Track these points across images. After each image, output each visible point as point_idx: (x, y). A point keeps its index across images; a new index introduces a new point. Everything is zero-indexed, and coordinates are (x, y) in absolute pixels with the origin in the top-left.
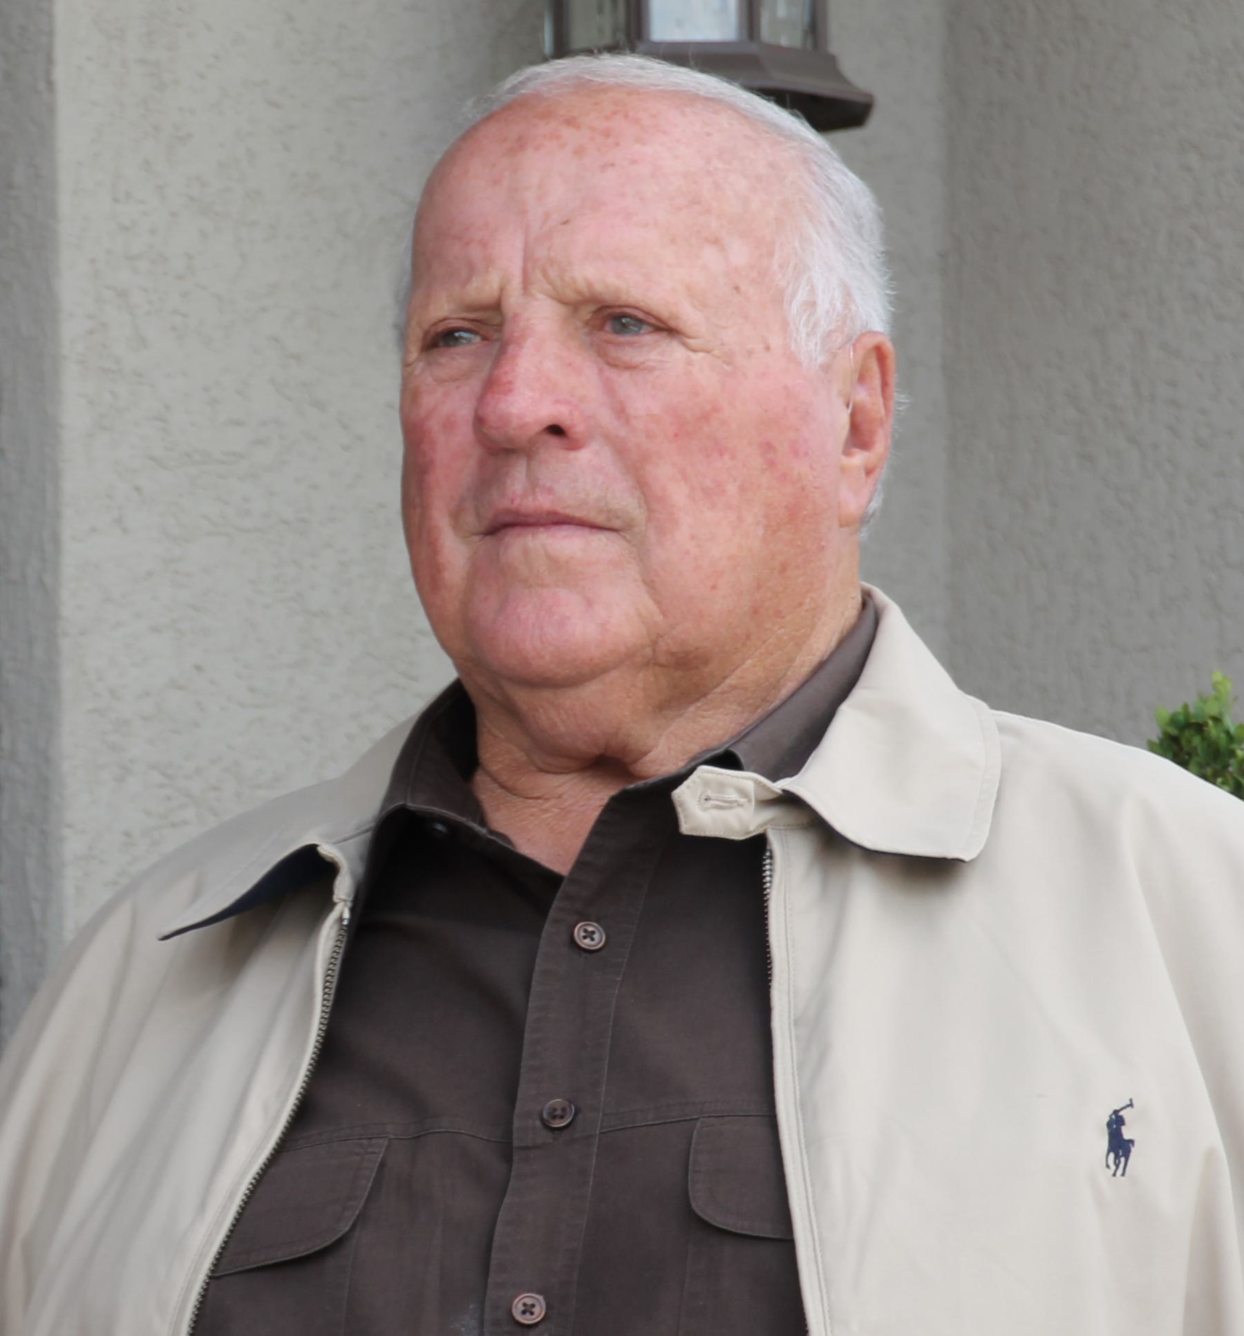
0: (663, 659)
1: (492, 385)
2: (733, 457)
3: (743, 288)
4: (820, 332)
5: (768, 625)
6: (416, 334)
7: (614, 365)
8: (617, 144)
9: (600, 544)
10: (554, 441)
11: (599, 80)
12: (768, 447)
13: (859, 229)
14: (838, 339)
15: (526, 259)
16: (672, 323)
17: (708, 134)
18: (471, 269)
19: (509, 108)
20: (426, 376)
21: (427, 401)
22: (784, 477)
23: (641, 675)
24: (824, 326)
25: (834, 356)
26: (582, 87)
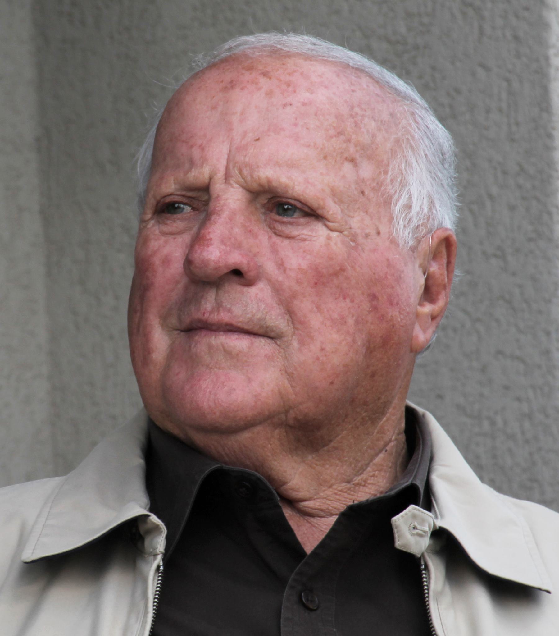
0: (291, 422)
1: (198, 239)
2: (352, 301)
3: (366, 193)
4: (412, 225)
5: (358, 410)
6: (151, 202)
7: (279, 235)
8: (295, 92)
9: (263, 346)
10: (235, 278)
11: (287, 49)
12: (373, 297)
13: (443, 162)
14: (424, 231)
15: (228, 160)
16: (320, 212)
17: (353, 91)
18: (192, 163)
19: (225, 61)
20: (154, 228)
21: (154, 244)
22: (382, 318)
23: (277, 431)
24: (415, 222)
25: (419, 241)
26: (276, 53)
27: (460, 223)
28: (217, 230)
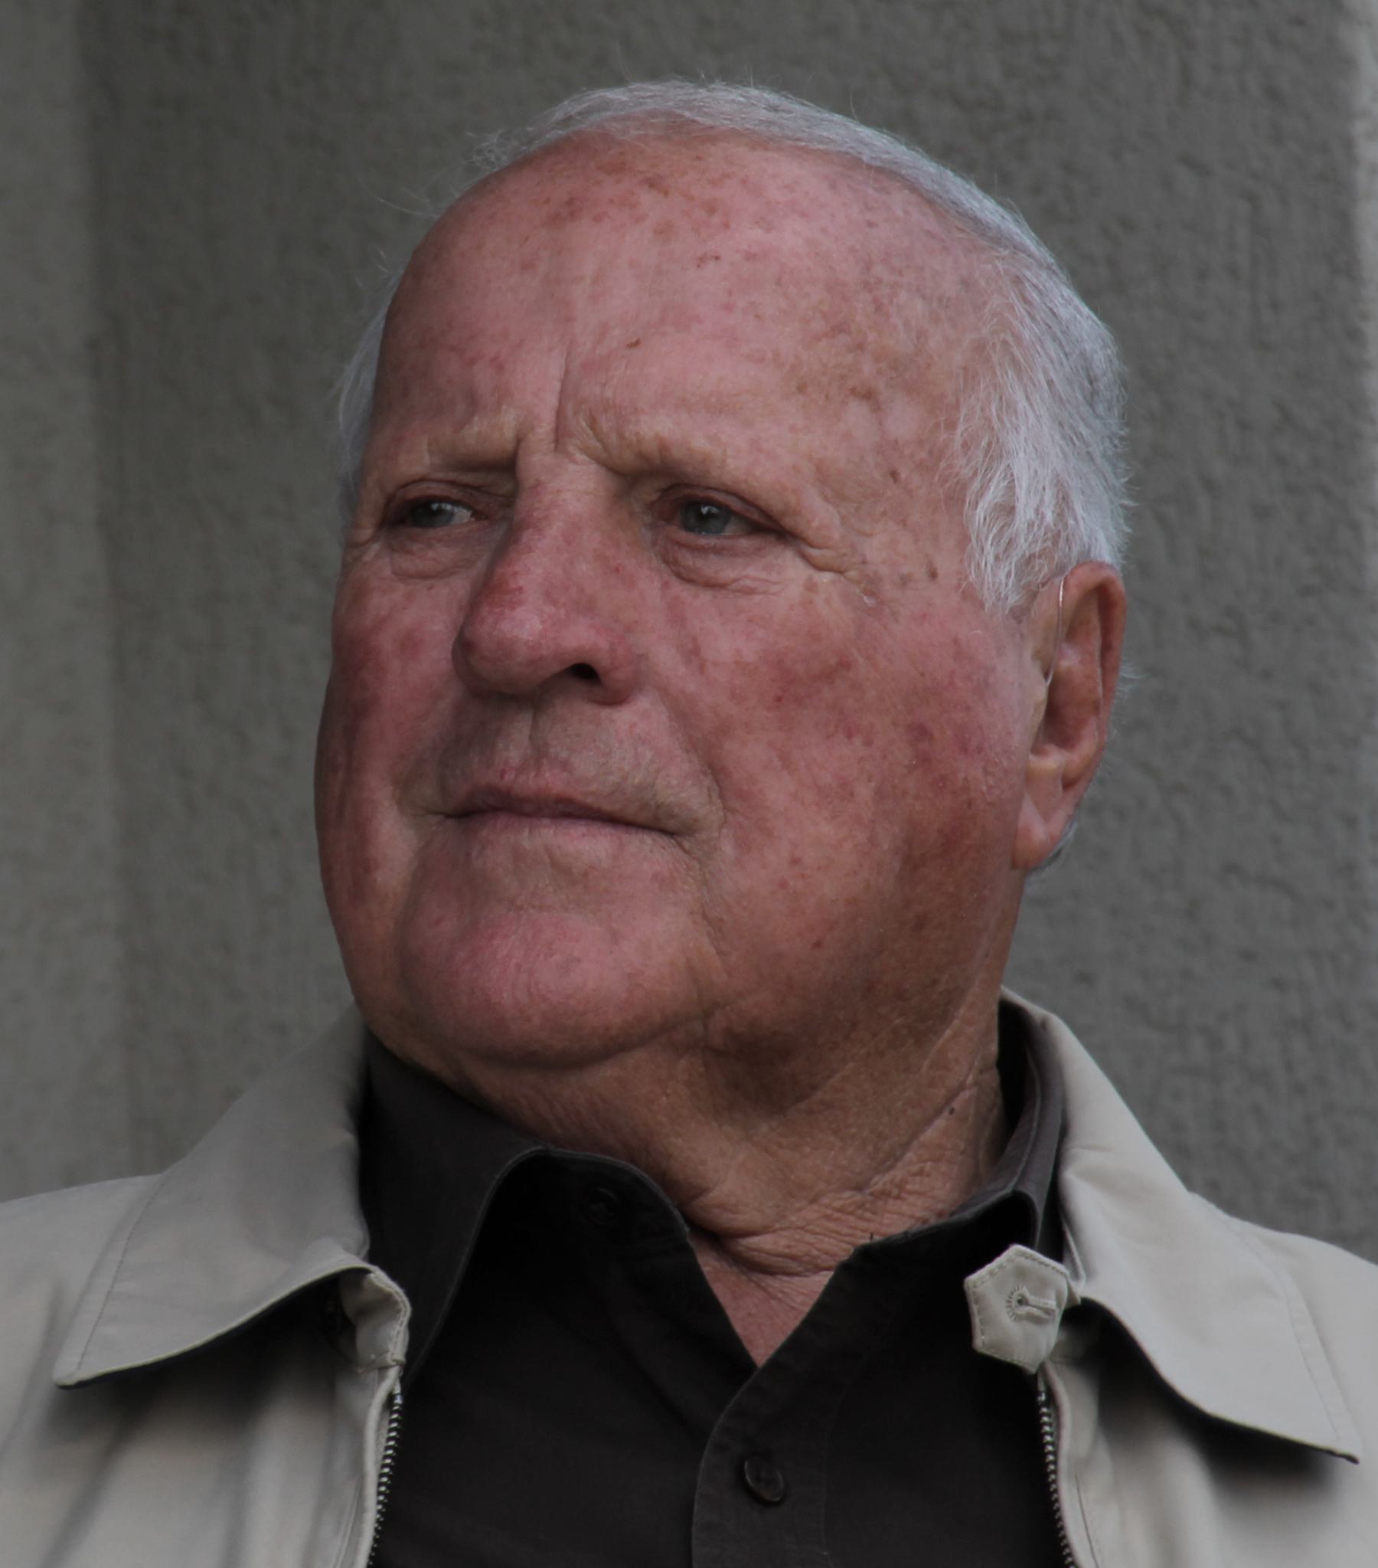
1: (489, 590)
2: (868, 743)
4: (1016, 556)
6: (373, 499)
7: (687, 578)
8: (727, 226)
9: (648, 854)
11: (708, 122)
12: (920, 732)
15: (563, 395)
16: (788, 522)
17: (871, 224)
18: (474, 402)
19: (555, 149)
20: (379, 562)
21: (378, 603)
23: (683, 1063)
24: (1023, 546)
26: (681, 131)
27: (1134, 550)
28: (536, 566)
